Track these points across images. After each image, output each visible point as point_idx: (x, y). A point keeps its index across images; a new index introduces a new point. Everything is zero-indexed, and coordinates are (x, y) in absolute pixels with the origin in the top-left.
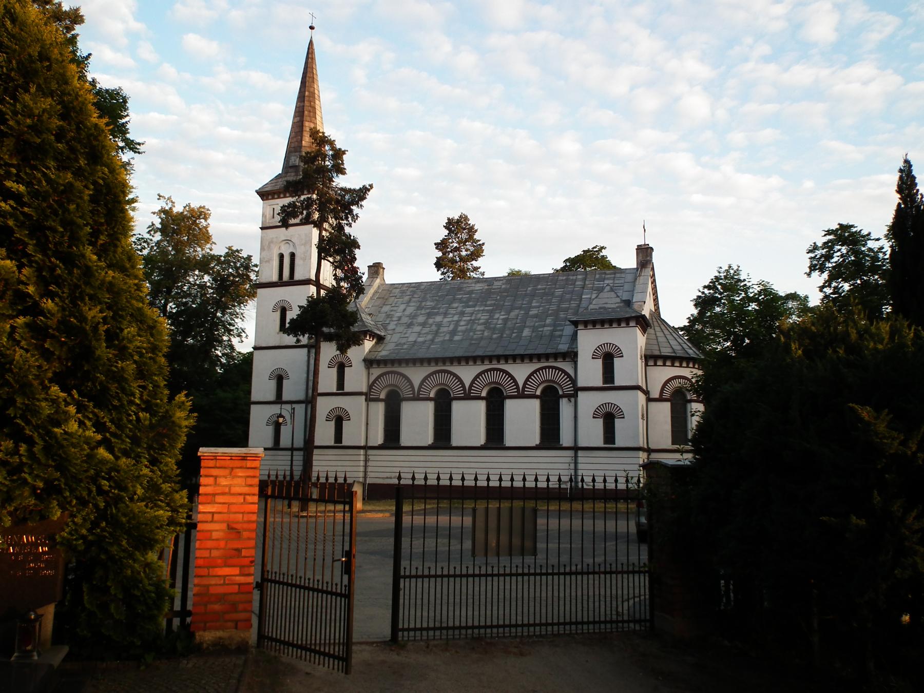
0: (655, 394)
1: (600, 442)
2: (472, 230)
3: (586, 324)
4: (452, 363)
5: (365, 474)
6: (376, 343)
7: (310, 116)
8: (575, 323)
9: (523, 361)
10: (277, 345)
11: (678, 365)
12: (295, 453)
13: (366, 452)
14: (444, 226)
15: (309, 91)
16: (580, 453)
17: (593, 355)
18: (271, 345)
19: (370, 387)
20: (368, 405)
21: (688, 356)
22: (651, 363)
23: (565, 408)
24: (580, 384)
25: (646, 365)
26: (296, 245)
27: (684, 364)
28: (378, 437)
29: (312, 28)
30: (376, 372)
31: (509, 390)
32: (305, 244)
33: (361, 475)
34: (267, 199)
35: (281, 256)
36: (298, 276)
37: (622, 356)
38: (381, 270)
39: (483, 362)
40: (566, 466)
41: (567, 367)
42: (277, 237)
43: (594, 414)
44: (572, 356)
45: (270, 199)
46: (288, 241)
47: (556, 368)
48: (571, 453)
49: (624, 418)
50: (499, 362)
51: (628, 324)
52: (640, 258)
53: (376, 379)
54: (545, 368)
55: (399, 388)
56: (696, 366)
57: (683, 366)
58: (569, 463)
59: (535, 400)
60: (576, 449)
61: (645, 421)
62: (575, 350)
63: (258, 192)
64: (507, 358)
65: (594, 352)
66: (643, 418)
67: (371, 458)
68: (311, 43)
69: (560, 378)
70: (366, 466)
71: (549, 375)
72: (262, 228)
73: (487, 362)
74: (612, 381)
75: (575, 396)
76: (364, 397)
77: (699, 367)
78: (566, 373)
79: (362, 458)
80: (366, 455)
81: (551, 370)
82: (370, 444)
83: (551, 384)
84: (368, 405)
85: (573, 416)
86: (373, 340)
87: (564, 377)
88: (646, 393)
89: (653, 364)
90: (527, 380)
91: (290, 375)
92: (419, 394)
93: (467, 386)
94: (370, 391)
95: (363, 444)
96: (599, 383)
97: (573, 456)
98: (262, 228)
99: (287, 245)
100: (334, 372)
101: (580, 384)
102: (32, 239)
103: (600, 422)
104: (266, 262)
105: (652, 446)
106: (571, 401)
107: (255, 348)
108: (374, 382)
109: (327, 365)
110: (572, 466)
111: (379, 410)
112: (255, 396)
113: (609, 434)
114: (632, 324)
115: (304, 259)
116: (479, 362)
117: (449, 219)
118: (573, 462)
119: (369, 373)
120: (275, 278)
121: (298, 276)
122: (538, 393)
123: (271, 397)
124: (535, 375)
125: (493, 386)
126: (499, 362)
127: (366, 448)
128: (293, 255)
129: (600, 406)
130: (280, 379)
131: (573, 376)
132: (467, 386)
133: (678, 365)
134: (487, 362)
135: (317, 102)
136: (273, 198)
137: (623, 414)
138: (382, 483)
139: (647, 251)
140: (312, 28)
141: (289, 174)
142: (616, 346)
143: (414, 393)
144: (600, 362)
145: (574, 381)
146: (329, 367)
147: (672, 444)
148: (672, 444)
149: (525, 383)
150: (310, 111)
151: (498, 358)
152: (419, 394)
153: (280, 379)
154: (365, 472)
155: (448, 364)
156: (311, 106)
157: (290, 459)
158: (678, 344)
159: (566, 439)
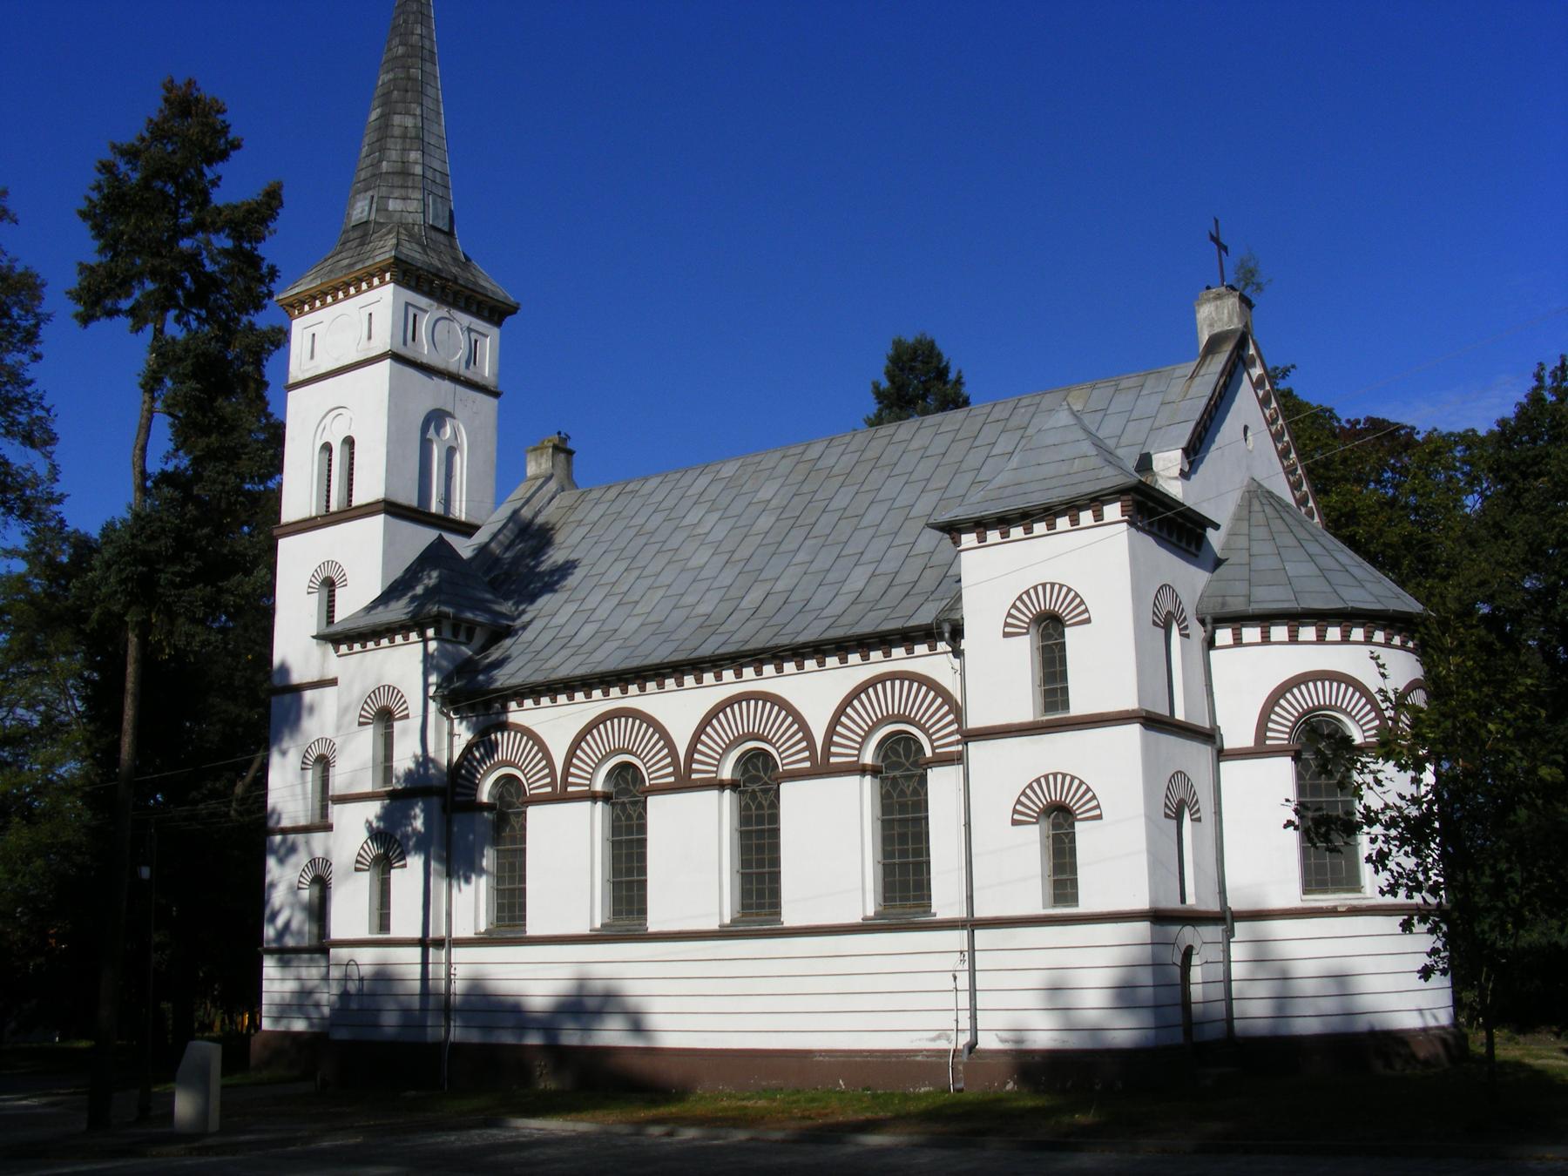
0: (1239, 733)
1: (1033, 901)
3: (980, 526)
8: (953, 530)
12: (960, 912)
16: (980, 934)
17: (1007, 624)
20: (449, 823)
22: (1224, 636)
24: (974, 721)
31: (788, 756)
35: (327, 447)
37: (1088, 621)
43: (1015, 811)
48: (958, 938)
49: (1099, 817)
60: (972, 924)
64: (778, 655)
71: (891, 699)
74: (1065, 705)
81: (915, 685)
84: (449, 823)
90: (836, 720)
92: (565, 783)
100: (1024, 650)
102: (133, 294)
116: (854, 658)
118: (966, 966)
122: (868, 758)
124: (924, 689)
128: (349, 442)
145: (958, 711)
146: (1006, 635)
149: (831, 731)
151: (757, 658)
152: (827, 752)
159: (945, 899)
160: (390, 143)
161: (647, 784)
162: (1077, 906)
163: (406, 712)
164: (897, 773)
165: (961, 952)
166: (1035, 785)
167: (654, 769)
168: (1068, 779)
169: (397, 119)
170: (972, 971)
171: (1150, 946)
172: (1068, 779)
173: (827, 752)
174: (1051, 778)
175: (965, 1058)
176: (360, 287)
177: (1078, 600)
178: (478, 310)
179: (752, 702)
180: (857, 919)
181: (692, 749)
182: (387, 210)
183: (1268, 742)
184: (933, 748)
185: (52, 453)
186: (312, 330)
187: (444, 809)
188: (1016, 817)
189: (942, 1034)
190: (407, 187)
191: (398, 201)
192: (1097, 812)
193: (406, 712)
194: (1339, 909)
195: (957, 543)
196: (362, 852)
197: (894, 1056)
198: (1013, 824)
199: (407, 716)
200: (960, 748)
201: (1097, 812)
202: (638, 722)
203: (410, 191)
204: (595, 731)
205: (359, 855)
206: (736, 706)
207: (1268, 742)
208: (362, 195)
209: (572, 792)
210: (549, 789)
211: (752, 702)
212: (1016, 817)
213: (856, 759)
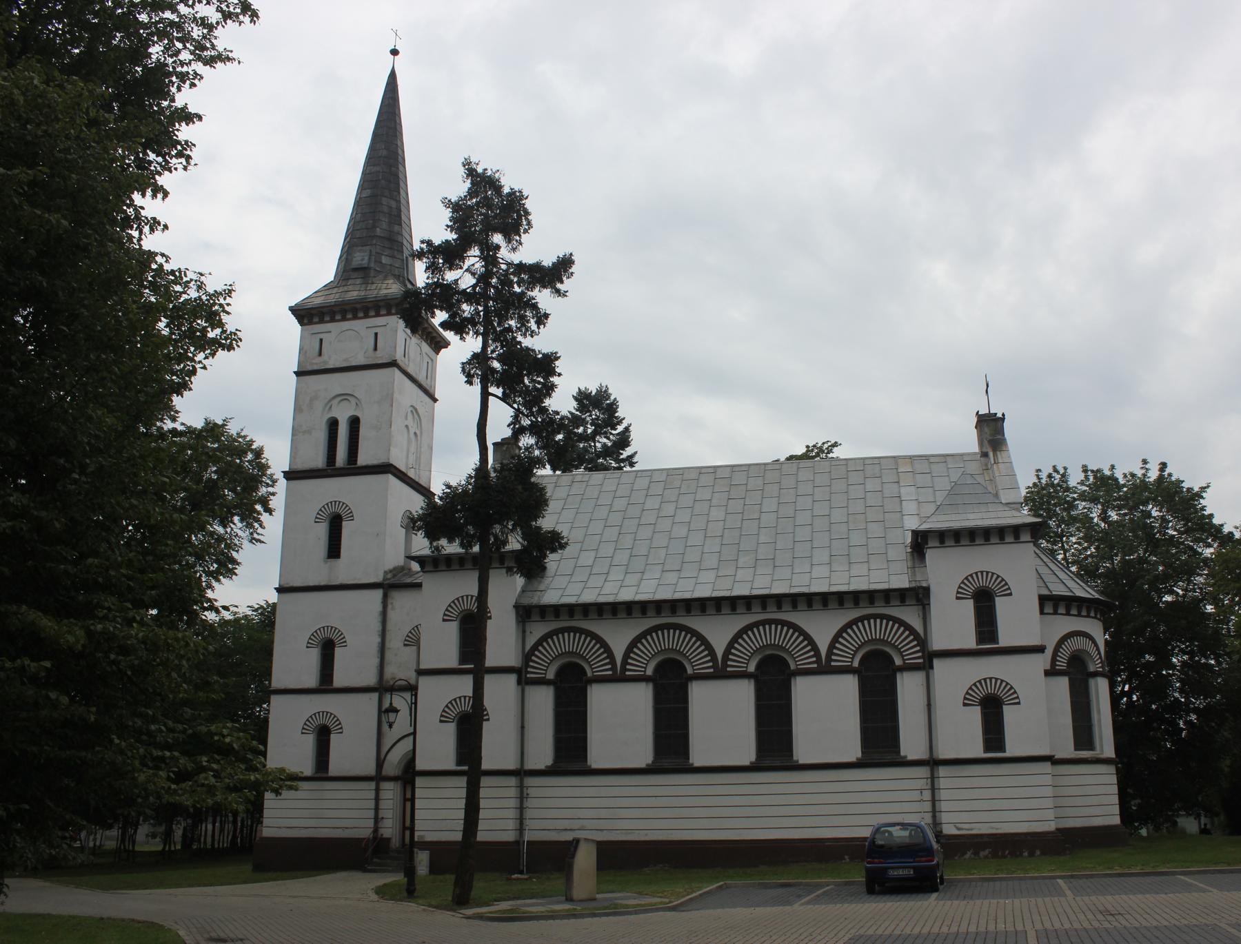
1: (976, 749)
2: (612, 408)
4: (795, 607)
5: (521, 823)
9: (718, 610)
10: (322, 584)
11: (1076, 613)
14: (573, 396)
16: (942, 771)
17: (958, 592)
18: (311, 584)
19: (527, 657)
21: (1071, 594)
23: (909, 688)
24: (937, 643)
27: (1062, 610)
28: (542, 752)
29: (395, 52)
30: (538, 630)
34: (311, 323)
35: (333, 425)
36: (363, 459)
40: (915, 795)
41: (911, 616)
44: (919, 596)
45: (316, 323)
46: (344, 397)
47: (889, 618)
50: (779, 607)
53: (539, 643)
54: (868, 617)
55: (584, 658)
56: (1092, 614)
57: (1059, 612)
58: (921, 791)
60: (933, 763)
62: (924, 584)
67: (532, 792)
68: (393, 76)
69: (896, 635)
71: (875, 630)
72: (298, 374)
73: (756, 608)
77: (1096, 614)
78: (908, 627)
87: (695, 643)
89: (1051, 611)
90: (835, 640)
91: (347, 638)
93: (719, 652)
94: (527, 666)
96: (971, 643)
98: (298, 374)
99: (345, 403)
101: (937, 643)
103: (976, 713)
104: (304, 432)
107: (280, 590)
108: (535, 647)
110: (927, 795)
111: (543, 701)
112: (279, 678)
113: (994, 733)
119: (524, 632)
120: (319, 461)
121: (363, 459)
123: (312, 681)
125: (769, 652)
126: (779, 607)
127: (521, 773)
128: (355, 423)
129: (975, 684)
130: (328, 648)
132: (719, 652)
133: (1076, 613)
136: (322, 321)
137: (1018, 697)
141: (350, 282)
143: (614, 668)
144: (969, 605)
145: (922, 642)
147: (1076, 749)
148: (1076, 749)
149: (832, 646)
152: (624, 669)
153: (328, 648)
155: (787, 606)
158: (1050, 572)
159: (911, 744)
162: (1005, 752)
168: (999, 682)
171: (940, 776)
172: (999, 682)
176: (391, 310)
177: (969, 578)
180: (643, 765)
181: (727, 652)
182: (381, 262)
183: (729, 669)
185: (632, 456)
186: (321, 336)
187: (519, 682)
192: (1017, 701)
207: (729, 669)
209: (629, 675)
210: (610, 673)
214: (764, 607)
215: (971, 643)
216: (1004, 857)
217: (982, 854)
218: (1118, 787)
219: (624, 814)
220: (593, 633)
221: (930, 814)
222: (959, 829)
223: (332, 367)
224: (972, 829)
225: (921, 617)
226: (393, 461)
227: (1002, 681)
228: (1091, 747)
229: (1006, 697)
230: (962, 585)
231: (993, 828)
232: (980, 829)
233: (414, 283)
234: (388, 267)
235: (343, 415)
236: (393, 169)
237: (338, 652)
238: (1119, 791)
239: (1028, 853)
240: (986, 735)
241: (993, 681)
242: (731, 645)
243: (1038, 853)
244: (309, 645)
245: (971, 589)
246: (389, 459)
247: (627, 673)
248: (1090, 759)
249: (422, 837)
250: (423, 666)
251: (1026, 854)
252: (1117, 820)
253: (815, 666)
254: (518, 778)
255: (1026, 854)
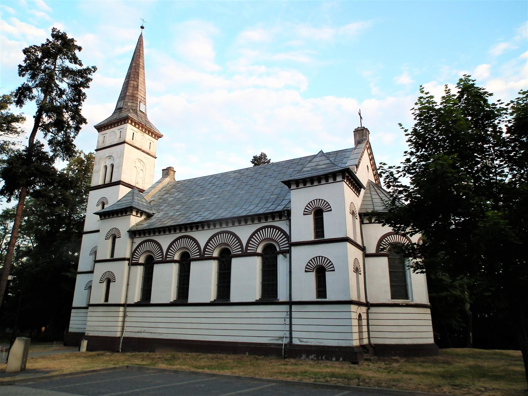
0: (372, 249)
1: (312, 296)
6: (145, 219)
7: (134, 78)
13: (125, 309)
15: (136, 63)
16: (294, 308)
19: (133, 254)
20: (130, 268)
23: (282, 262)
24: (294, 240)
25: (362, 223)
26: (115, 159)
29: (142, 27)
30: (138, 241)
32: (119, 158)
33: (120, 329)
34: (101, 131)
35: (106, 167)
37: (331, 210)
38: (172, 172)
39: (215, 226)
40: (282, 321)
41: (282, 224)
42: (104, 155)
43: (306, 268)
46: (110, 157)
48: (286, 308)
49: (334, 270)
50: (227, 225)
51: (335, 179)
52: (358, 138)
53: (138, 247)
59: (256, 257)
60: (290, 303)
61: (361, 277)
62: (289, 209)
63: (95, 127)
65: (305, 209)
66: (357, 270)
68: (141, 36)
69: (277, 236)
70: (124, 322)
71: (268, 233)
73: (218, 226)
74: (323, 236)
75: (289, 251)
76: (127, 262)
79: (121, 314)
80: (125, 312)
82: (129, 302)
83: (270, 242)
85: (288, 271)
86: (141, 216)
88: (363, 249)
92: (166, 257)
95: (122, 302)
97: (288, 310)
101: (294, 240)
103: (312, 276)
105: (371, 301)
106: (286, 257)
108: (136, 249)
109: (105, 238)
110: (288, 321)
114: (339, 179)
115: (118, 168)
117: (254, 157)
125: (223, 247)
128: (112, 166)
131: (288, 233)
134: (218, 226)
135: (141, 70)
137: (333, 267)
138: (134, 336)
139: (363, 132)
140: (142, 27)
142: (325, 201)
144: (311, 218)
147: (392, 299)
148: (392, 299)
150: (135, 75)
152: (247, 249)
154: (123, 327)
156: (136, 72)
157: (288, 329)
159: (282, 296)
160: (129, 88)
161: (191, 258)
163: (120, 236)
164: (268, 256)
165: (287, 312)
166: (313, 260)
167: (194, 253)
168: (323, 258)
169: (132, 82)
170: (291, 318)
173: (247, 249)
174: (318, 258)
175: (288, 346)
177: (328, 204)
178: (145, 131)
179: (225, 234)
181: (205, 247)
182: (128, 105)
184: (280, 248)
187: (129, 264)
188: (306, 270)
189: (281, 338)
190: (134, 100)
191: (131, 103)
192: (333, 269)
193: (120, 236)
194: (404, 304)
195: (290, 187)
196: (102, 277)
197: (265, 345)
198: (305, 272)
199: (120, 237)
200: (288, 248)
201: (333, 269)
202: (153, 243)
203: (134, 101)
204: (176, 242)
205: (101, 278)
206: (220, 235)
207: (205, 256)
208: (121, 101)
210: (161, 259)
211: (269, 229)
212: (306, 270)
213: (256, 251)
214: (221, 225)
215: (311, 237)
216: (322, 359)
217: (311, 357)
218: (432, 321)
219: (160, 325)
220: (157, 242)
221: (289, 332)
222: (301, 341)
223: (106, 146)
224: (307, 342)
225: (288, 224)
226: (122, 180)
227: (325, 258)
228: (407, 297)
229: (327, 267)
230: (307, 207)
231: (319, 342)
232: (312, 342)
233: (313, 157)
234: (131, 107)
235: (108, 163)
236: (137, 70)
237: (329, 275)
238: (432, 324)
239: (336, 359)
240: (318, 288)
241: (321, 258)
242: (207, 244)
243: (341, 359)
244: (90, 254)
245: (314, 206)
246: (121, 179)
247: (167, 259)
248: (401, 304)
249: (88, 333)
250: (97, 259)
251: (334, 359)
252: (431, 341)
253: (241, 252)
254: (124, 308)
255: (334, 359)
